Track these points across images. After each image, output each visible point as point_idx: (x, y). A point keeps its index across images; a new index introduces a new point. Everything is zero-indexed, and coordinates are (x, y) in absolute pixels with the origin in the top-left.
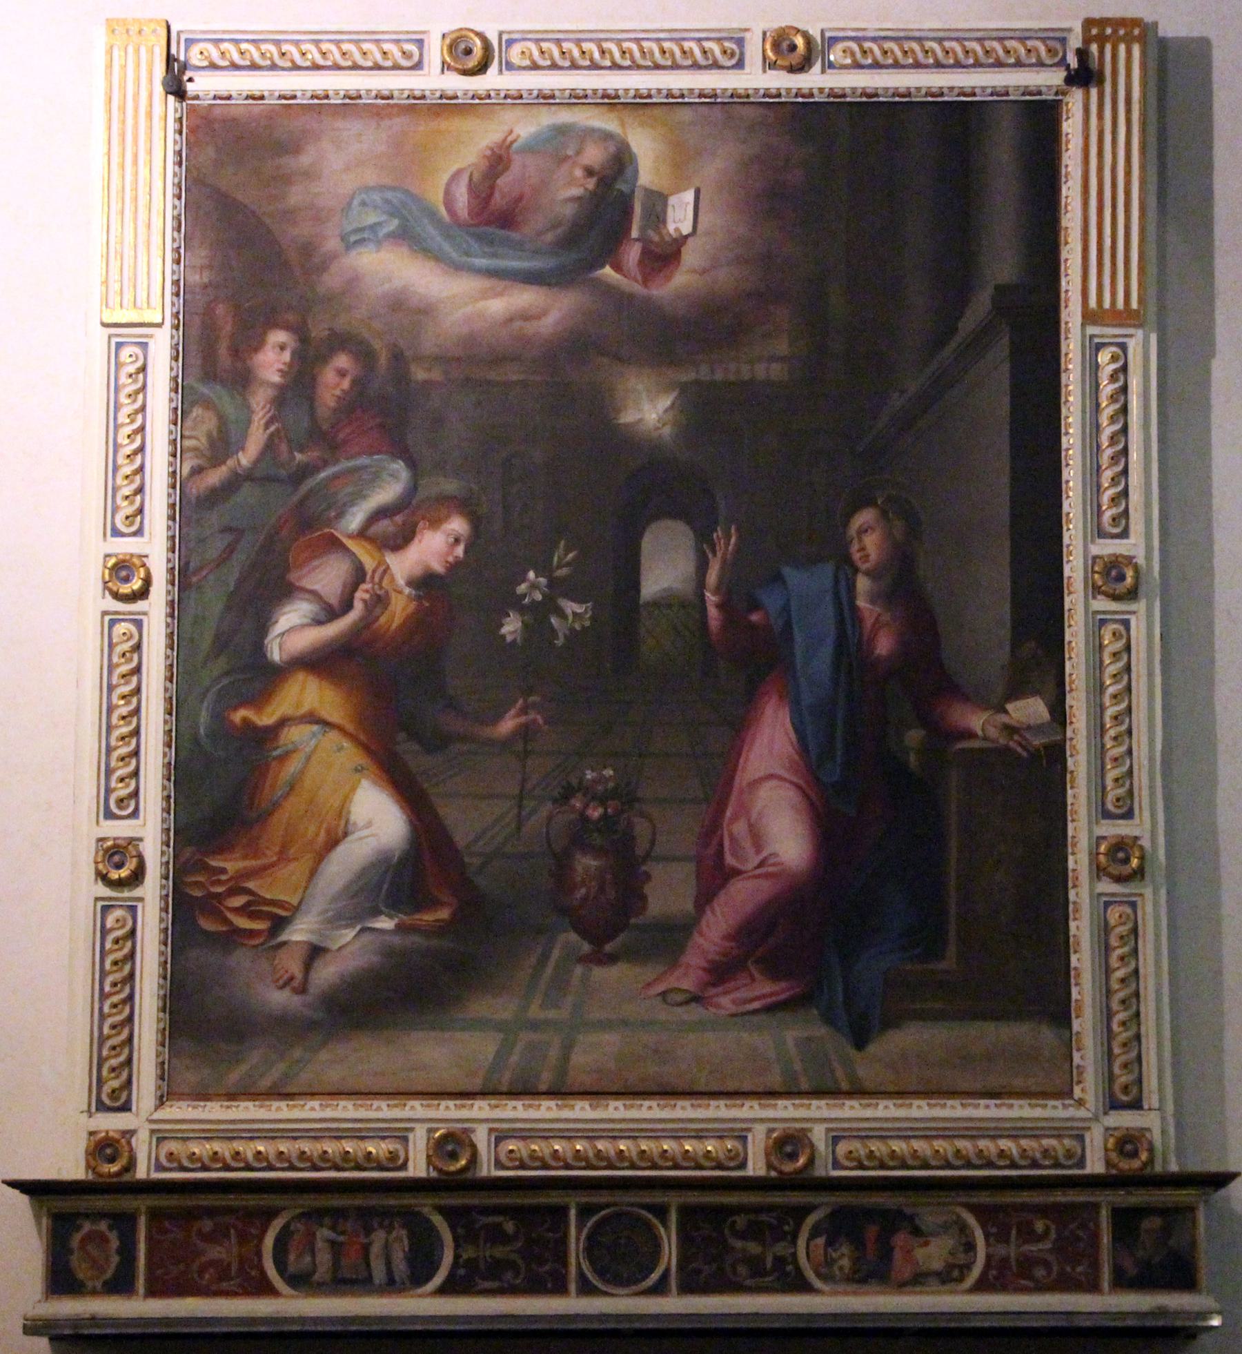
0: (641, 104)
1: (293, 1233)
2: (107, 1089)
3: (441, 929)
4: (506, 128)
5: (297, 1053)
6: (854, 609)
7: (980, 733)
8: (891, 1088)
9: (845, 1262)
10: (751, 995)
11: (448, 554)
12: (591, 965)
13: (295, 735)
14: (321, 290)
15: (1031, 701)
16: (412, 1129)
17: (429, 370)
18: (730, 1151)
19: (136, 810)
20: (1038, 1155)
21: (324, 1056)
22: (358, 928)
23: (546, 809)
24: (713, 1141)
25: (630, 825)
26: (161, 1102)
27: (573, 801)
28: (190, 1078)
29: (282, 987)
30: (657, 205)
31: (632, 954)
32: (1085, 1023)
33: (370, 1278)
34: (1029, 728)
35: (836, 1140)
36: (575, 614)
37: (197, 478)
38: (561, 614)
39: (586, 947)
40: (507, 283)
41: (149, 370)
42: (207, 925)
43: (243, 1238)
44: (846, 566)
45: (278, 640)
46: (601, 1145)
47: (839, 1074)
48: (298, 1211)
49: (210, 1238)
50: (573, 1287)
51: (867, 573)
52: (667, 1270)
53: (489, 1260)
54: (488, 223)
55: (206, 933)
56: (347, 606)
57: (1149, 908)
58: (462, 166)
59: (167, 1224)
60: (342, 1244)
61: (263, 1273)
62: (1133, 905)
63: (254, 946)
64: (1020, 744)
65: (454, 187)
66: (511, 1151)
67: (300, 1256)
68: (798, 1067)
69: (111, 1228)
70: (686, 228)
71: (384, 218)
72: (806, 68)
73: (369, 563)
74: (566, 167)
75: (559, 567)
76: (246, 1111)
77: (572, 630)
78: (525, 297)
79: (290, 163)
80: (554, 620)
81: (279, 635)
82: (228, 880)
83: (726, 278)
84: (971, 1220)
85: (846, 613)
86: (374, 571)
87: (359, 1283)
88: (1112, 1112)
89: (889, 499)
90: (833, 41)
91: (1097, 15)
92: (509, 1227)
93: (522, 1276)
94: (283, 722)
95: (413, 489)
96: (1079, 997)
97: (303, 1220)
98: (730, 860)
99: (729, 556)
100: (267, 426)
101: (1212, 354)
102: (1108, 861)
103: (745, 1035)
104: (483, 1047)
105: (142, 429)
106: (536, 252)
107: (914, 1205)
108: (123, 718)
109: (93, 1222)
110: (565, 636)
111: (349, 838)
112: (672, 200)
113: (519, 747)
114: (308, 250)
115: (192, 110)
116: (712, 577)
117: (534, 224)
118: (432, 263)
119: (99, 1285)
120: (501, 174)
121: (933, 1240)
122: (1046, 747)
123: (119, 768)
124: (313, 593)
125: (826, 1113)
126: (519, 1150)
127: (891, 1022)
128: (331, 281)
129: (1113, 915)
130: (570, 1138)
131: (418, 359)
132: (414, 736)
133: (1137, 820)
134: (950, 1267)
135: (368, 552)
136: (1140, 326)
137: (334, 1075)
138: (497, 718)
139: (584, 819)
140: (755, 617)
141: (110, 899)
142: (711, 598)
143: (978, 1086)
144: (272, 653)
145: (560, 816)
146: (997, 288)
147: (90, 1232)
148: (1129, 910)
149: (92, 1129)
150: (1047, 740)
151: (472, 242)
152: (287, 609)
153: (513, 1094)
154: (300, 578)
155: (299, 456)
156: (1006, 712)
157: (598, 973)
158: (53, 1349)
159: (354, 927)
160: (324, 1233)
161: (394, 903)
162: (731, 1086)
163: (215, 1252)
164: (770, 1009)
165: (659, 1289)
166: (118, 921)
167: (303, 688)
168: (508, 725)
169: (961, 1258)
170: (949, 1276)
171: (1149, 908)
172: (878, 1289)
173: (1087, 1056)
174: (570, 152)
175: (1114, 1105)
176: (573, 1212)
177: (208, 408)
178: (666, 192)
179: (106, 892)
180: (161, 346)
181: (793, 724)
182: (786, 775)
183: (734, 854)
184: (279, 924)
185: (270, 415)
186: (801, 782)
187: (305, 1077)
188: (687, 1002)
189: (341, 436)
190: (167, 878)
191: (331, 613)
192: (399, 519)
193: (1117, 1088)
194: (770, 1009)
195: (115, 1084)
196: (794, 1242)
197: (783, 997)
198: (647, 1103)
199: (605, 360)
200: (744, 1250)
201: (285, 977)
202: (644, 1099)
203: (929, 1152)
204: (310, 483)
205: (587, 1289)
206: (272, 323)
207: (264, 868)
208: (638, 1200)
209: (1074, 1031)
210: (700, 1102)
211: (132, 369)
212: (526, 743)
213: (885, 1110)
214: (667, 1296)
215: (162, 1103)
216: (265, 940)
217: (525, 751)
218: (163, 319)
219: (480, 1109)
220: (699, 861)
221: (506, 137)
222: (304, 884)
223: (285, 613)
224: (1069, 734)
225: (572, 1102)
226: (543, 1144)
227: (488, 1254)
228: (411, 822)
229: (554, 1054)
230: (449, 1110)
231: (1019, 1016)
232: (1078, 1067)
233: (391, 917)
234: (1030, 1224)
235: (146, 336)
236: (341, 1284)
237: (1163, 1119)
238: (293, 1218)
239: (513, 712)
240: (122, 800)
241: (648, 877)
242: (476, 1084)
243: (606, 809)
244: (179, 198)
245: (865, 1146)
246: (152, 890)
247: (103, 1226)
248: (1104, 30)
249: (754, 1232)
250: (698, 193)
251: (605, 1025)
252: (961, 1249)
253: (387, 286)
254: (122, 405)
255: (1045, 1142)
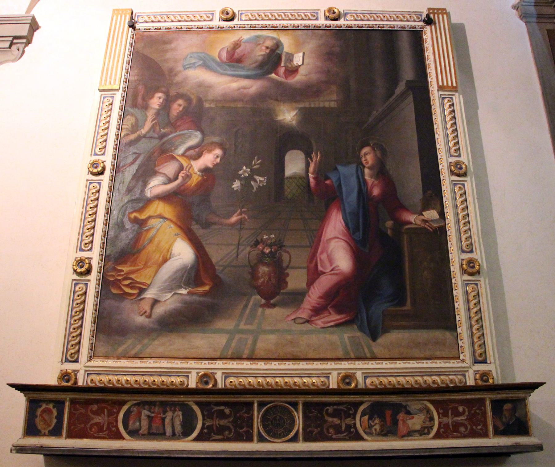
0: (285, 29)
1: (132, 412)
2: (69, 353)
3: (206, 294)
4: (240, 37)
5: (146, 341)
6: (365, 180)
7: (414, 222)
8: (387, 356)
9: (377, 427)
10: (330, 319)
11: (214, 161)
12: (265, 308)
13: (153, 222)
14: (175, 81)
15: (432, 211)
16: (190, 372)
17: (210, 104)
18: (322, 382)
19: (92, 248)
20: (448, 382)
21: (156, 342)
22: (173, 293)
23: (248, 249)
24: (316, 378)
25: (281, 255)
26: (90, 359)
27: (258, 246)
28: (101, 349)
29: (141, 315)
30: (290, 57)
31: (283, 304)
32: (463, 329)
33: (164, 434)
34: (432, 221)
35: (366, 377)
36: (260, 181)
37: (126, 137)
38: (255, 181)
39: (263, 301)
40: (238, 78)
41: (113, 104)
42: (115, 291)
43: (110, 414)
44: (360, 166)
45: (150, 190)
46: (269, 380)
47: (366, 350)
48: (135, 402)
49: (97, 413)
50: (255, 438)
51: (368, 168)
52: (298, 431)
53: (218, 426)
54: (232, 62)
55: (114, 294)
56: (176, 178)
57: (483, 285)
58: (224, 46)
59: (78, 406)
60: (153, 417)
61: (118, 429)
62: (476, 284)
63: (132, 299)
64: (429, 226)
65: (222, 52)
66: (231, 382)
67: (134, 423)
68: (349, 348)
69: (54, 407)
70: (300, 63)
71: (198, 61)
72: (339, 20)
73: (185, 165)
74: (259, 47)
75: (255, 165)
76: (124, 363)
77: (259, 186)
78: (245, 83)
79: (168, 46)
80: (252, 183)
81: (150, 188)
82: (124, 274)
83: (314, 77)
84: (431, 407)
85: (362, 182)
86: (187, 167)
87: (160, 435)
88: (476, 365)
89: (374, 144)
90: (347, 13)
91: (432, 7)
92: (227, 411)
93: (232, 434)
94: (150, 217)
95: (202, 140)
96: (460, 319)
97: (136, 407)
98: (320, 268)
99: (317, 162)
100: (152, 122)
101: (477, 108)
102: (467, 267)
103: (328, 336)
104: (220, 340)
105: (109, 122)
106: (249, 70)
107: (406, 401)
108: (90, 215)
109: (47, 404)
110: (256, 188)
111: (170, 260)
112: (295, 55)
113: (238, 227)
114: (171, 70)
115: (137, 33)
116: (311, 169)
117: (248, 62)
118: (213, 73)
119: (47, 432)
120: (237, 49)
121: (416, 416)
122: (439, 227)
123: (87, 232)
124: (164, 174)
125: (361, 366)
126: (234, 381)
127: (386, 330)
128: (178, 79)
129: (469, 289)
130: (256, 377)
131: (206, 100)
132: (198, 222)
133: (475, 253)
134: (423, 428)
135: (184, 160)
136: (456, 92)
137: (161, 350)
138: (230, 216)
139: (263, 252)
140: (328, 182)
141: (78, 280)
142: (311, 176)
143: (422, 355)
144: (147, 194)
145: (253, 252)
146: (407, 81)
147: (45, 408)
148: (475, 286)
149: (61, 369)
150: (439, 225)
151: (227, 67)
152: (154, 179)
153: (232, 359)
154: (159, 169)
155: (162, 131)
156: (423, 215)
157: (268, 311)
158: (46, 461)
159: (171, 293)
160: (145, 412)
161: (187, 284)
162: (322, 356)
163: (97, 419)
164: (337, 325)
165: (294, 439)
166: (80, 288)
167: (158, 205)
168: (234, 219)
169: (428, 424)
170: (423, 432)
171: (483, 285)
172: (392, 438)
173: (465, 342)
174: (261, 42)
175: (476, 362)
176: (256, 405)
177: (132, 116)
178: (293, 53)
179: (76, 277)
180: (118, 96)
181: (343, 220)
182: (340, 236)
183: (322, 266)
184: (142, 291)
185: (153, 118)
186: (348, 240)
187: (149, 350)
188: (304, 323)
189: (178, 124)
190: (100, 273)
191: (170, 181)
192: (197, 150)
193: (477, 355)
194: (337, 325)
195: (73, 351)
196: (354, 418)
197: (342, 321)
198: (287, 363)
199: (272, 101)
200: (332, 422)
201: (144, 311)
202: (286, 361)
203: (404, 382)
204: (165, 139)
205: (262, 439)
206: (157, 90)
207: (138, 270)
208: (284, 399)
209: (459, 333)
210: (310, 362)
211: (107, 104)
212: (241, 225)
213: (386, 365)
214: (298, 443)
215: (91, 360)
216: (136, 297)
217: (241, 228)
218: (120, 88)
219: (219, 364)
220: (308, 268)
221: (239, 39)
222: (152, 276)
223: (153, 181)
224: (447, 222)
225: (257, 362)
226: (244, 379)
227: (217, 423)
228: (195, 254)
229: (250, 342)
230: (206, 365)
231: (437, 327)
232: (462, 346)
233: (186, 289)
234: (456, 408)
235: (114, 94)
236: (151, 435)
237: (496, 367)
238: (132, 405)
239: (236, 214)
240: (86, 244)
241: (288, 275)
242: (218, 354)
243: (271, 249)
244: (130, 56)
245: (378, 379)
246: (93, 277)
247: (51, 406)
248: (434, 11)
249: (336, 414)
250: (304, 53)
251: (271, 332)
252: (428, 419)
253: (197, 80)
254: (102, 114)
255: (451, 377)
